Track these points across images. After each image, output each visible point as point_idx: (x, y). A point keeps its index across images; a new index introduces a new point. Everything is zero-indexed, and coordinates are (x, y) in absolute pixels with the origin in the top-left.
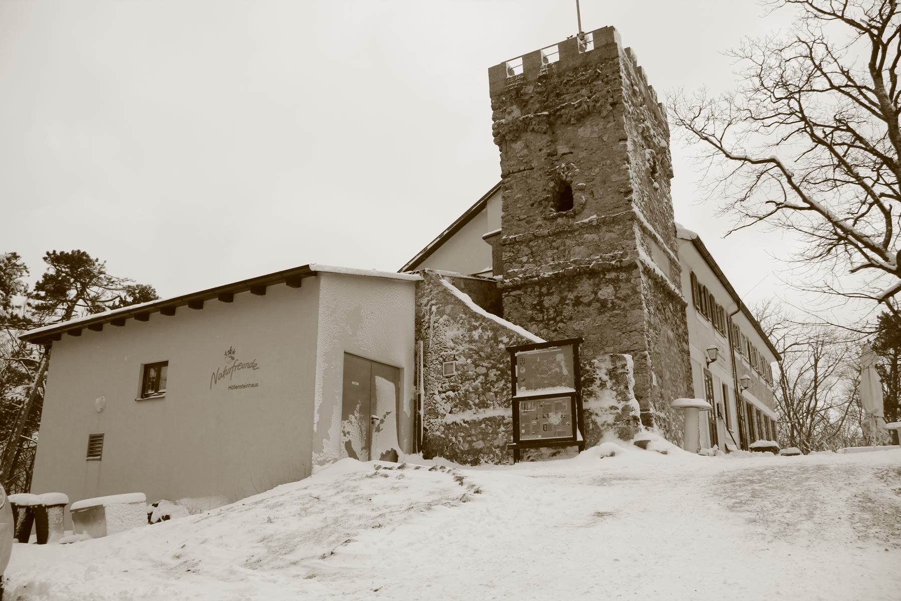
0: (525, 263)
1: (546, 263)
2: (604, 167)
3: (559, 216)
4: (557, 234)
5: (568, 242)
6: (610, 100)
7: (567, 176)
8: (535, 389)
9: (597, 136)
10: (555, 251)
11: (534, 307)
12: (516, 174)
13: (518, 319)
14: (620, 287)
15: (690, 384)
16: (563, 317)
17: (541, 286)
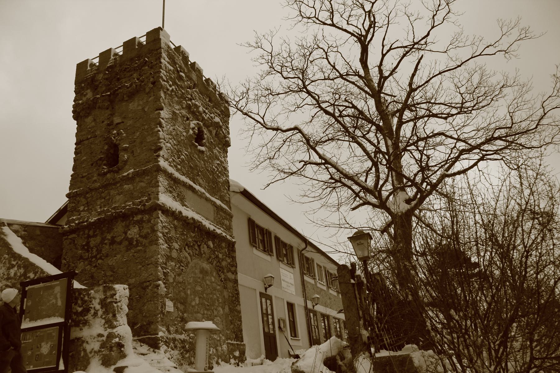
0: (82, 211)
1: (96, 210)
5: (113, 192)
6: (152, 80)
7: (117, 140)
8: (36, 320)
10: (103, 200)
11: (83, 247)
12: (85, 142)
14: (143, 227)
16: (102, 255)
17: (90, 230)
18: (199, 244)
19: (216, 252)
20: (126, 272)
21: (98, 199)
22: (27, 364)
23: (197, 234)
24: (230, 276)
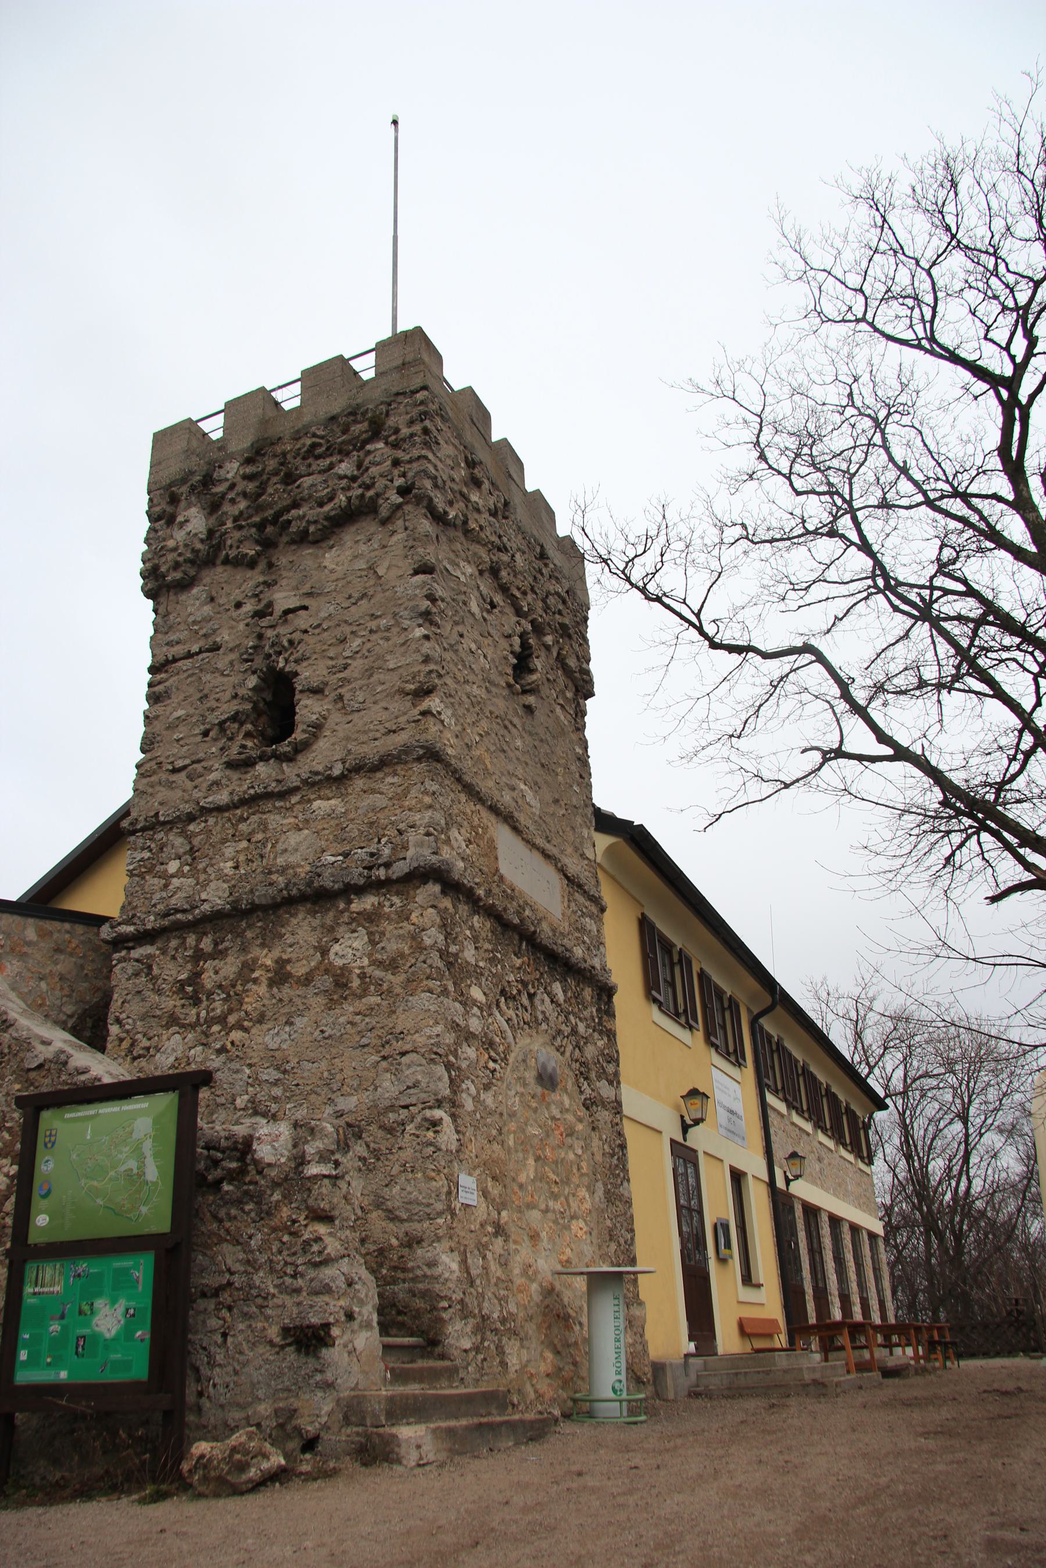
0: (172, 876)
2: (374, 637)
3: (264, 758)
4: (250, 801)
5: (274, 820)
6: (399, 482)
9: (364, 567)
10: (244, 844)
12: (180, 664)
13: (142, 1019)
18: (532, 991)
19: (571, 1017)
20: (326, 1074)
21: (226, 840)
22: (49, 1364)
23: (526, 959)
24: (606, 1090)
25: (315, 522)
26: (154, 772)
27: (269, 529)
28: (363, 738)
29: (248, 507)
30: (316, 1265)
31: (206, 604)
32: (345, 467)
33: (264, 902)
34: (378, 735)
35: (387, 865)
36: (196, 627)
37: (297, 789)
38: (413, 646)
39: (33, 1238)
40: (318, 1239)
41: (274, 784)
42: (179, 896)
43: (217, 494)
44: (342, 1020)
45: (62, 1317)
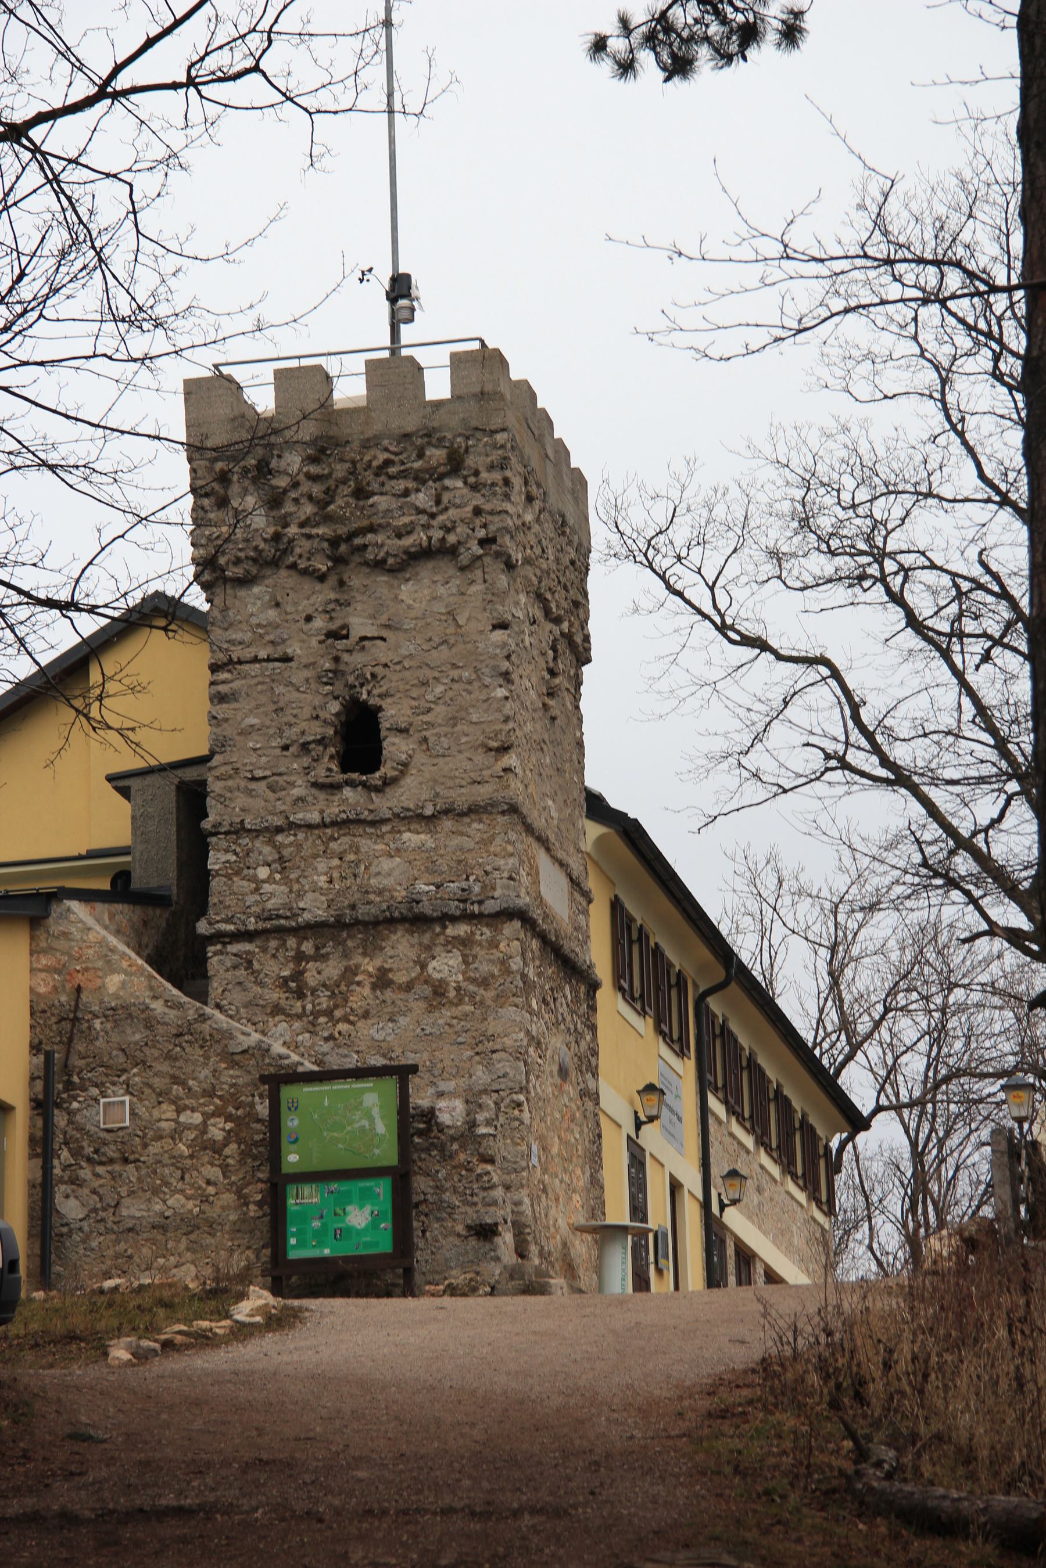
0: (263, 881)
2: (455, 686)
5: (366, 844)
6: (482, 533)
9: (444, 611)
12: (246, 667)
13: (245, 1007)
15: (597, 1172)
25: (395, 556)
26: (230, 777)
27: (343, 548)
28: (450, 783)
29: (316, 514)
30: (485, 1189)
31: (271, 607)
32: (422, 499)
33: (367, 918)
34: (464, 783)
35: (480, 903)
36: (260, 631)
37: (389, 820)
38: (495, 706)
39: (285, 1169)
40: (488, 1173)
41: (366, 813)
42: (276, 896)
43: (278, 487)
44: (441, 1021)
45: (322, 1217)
